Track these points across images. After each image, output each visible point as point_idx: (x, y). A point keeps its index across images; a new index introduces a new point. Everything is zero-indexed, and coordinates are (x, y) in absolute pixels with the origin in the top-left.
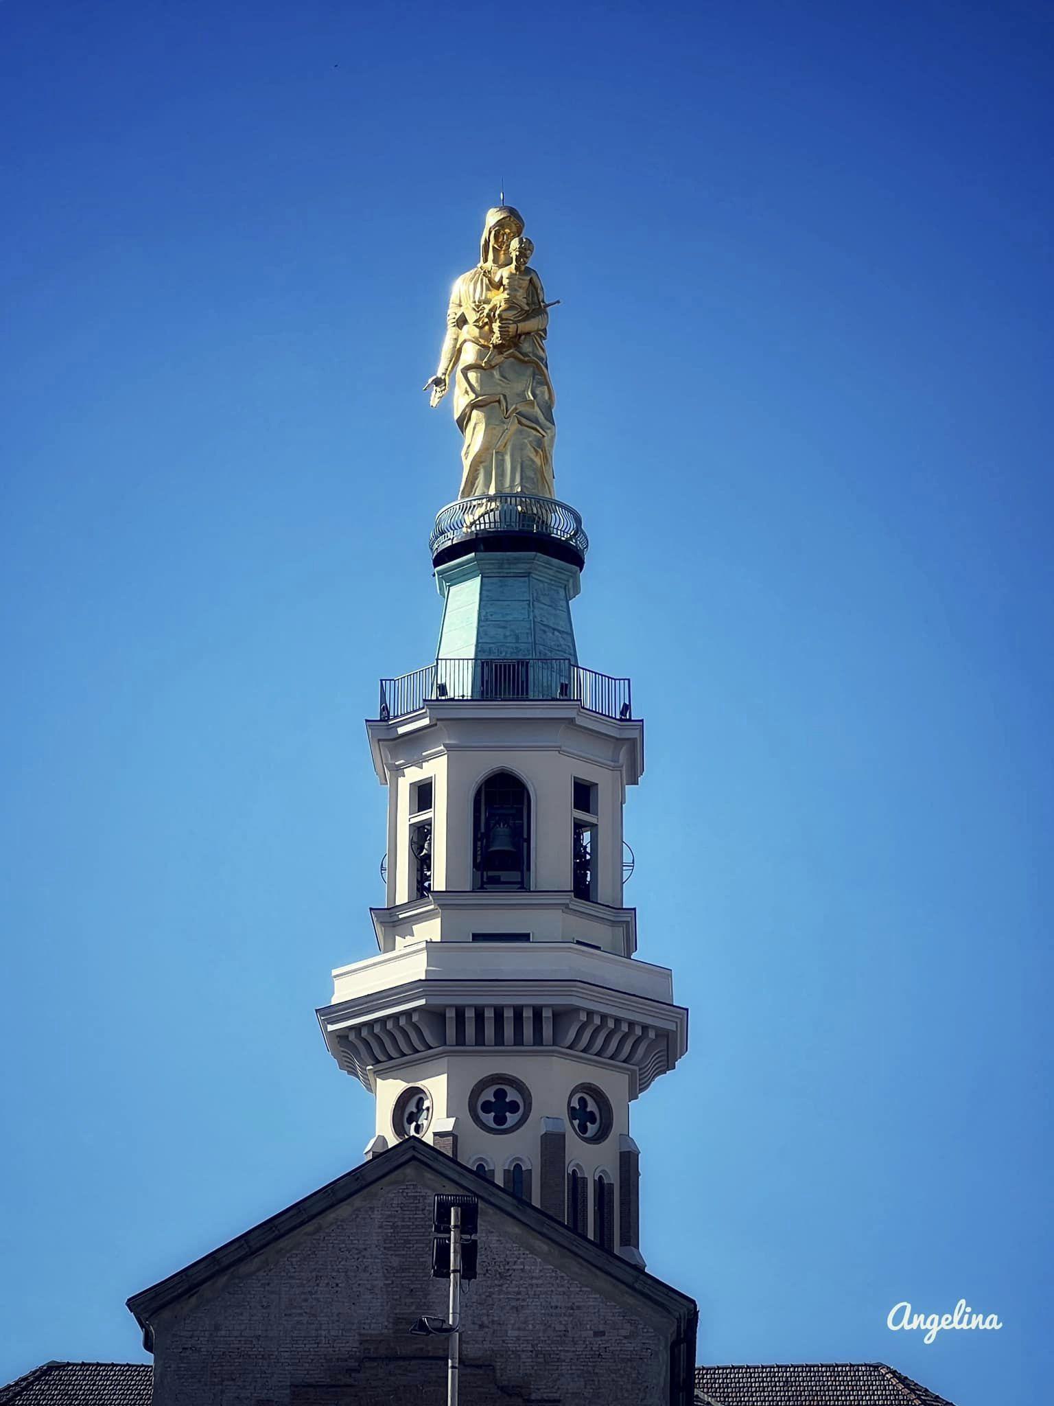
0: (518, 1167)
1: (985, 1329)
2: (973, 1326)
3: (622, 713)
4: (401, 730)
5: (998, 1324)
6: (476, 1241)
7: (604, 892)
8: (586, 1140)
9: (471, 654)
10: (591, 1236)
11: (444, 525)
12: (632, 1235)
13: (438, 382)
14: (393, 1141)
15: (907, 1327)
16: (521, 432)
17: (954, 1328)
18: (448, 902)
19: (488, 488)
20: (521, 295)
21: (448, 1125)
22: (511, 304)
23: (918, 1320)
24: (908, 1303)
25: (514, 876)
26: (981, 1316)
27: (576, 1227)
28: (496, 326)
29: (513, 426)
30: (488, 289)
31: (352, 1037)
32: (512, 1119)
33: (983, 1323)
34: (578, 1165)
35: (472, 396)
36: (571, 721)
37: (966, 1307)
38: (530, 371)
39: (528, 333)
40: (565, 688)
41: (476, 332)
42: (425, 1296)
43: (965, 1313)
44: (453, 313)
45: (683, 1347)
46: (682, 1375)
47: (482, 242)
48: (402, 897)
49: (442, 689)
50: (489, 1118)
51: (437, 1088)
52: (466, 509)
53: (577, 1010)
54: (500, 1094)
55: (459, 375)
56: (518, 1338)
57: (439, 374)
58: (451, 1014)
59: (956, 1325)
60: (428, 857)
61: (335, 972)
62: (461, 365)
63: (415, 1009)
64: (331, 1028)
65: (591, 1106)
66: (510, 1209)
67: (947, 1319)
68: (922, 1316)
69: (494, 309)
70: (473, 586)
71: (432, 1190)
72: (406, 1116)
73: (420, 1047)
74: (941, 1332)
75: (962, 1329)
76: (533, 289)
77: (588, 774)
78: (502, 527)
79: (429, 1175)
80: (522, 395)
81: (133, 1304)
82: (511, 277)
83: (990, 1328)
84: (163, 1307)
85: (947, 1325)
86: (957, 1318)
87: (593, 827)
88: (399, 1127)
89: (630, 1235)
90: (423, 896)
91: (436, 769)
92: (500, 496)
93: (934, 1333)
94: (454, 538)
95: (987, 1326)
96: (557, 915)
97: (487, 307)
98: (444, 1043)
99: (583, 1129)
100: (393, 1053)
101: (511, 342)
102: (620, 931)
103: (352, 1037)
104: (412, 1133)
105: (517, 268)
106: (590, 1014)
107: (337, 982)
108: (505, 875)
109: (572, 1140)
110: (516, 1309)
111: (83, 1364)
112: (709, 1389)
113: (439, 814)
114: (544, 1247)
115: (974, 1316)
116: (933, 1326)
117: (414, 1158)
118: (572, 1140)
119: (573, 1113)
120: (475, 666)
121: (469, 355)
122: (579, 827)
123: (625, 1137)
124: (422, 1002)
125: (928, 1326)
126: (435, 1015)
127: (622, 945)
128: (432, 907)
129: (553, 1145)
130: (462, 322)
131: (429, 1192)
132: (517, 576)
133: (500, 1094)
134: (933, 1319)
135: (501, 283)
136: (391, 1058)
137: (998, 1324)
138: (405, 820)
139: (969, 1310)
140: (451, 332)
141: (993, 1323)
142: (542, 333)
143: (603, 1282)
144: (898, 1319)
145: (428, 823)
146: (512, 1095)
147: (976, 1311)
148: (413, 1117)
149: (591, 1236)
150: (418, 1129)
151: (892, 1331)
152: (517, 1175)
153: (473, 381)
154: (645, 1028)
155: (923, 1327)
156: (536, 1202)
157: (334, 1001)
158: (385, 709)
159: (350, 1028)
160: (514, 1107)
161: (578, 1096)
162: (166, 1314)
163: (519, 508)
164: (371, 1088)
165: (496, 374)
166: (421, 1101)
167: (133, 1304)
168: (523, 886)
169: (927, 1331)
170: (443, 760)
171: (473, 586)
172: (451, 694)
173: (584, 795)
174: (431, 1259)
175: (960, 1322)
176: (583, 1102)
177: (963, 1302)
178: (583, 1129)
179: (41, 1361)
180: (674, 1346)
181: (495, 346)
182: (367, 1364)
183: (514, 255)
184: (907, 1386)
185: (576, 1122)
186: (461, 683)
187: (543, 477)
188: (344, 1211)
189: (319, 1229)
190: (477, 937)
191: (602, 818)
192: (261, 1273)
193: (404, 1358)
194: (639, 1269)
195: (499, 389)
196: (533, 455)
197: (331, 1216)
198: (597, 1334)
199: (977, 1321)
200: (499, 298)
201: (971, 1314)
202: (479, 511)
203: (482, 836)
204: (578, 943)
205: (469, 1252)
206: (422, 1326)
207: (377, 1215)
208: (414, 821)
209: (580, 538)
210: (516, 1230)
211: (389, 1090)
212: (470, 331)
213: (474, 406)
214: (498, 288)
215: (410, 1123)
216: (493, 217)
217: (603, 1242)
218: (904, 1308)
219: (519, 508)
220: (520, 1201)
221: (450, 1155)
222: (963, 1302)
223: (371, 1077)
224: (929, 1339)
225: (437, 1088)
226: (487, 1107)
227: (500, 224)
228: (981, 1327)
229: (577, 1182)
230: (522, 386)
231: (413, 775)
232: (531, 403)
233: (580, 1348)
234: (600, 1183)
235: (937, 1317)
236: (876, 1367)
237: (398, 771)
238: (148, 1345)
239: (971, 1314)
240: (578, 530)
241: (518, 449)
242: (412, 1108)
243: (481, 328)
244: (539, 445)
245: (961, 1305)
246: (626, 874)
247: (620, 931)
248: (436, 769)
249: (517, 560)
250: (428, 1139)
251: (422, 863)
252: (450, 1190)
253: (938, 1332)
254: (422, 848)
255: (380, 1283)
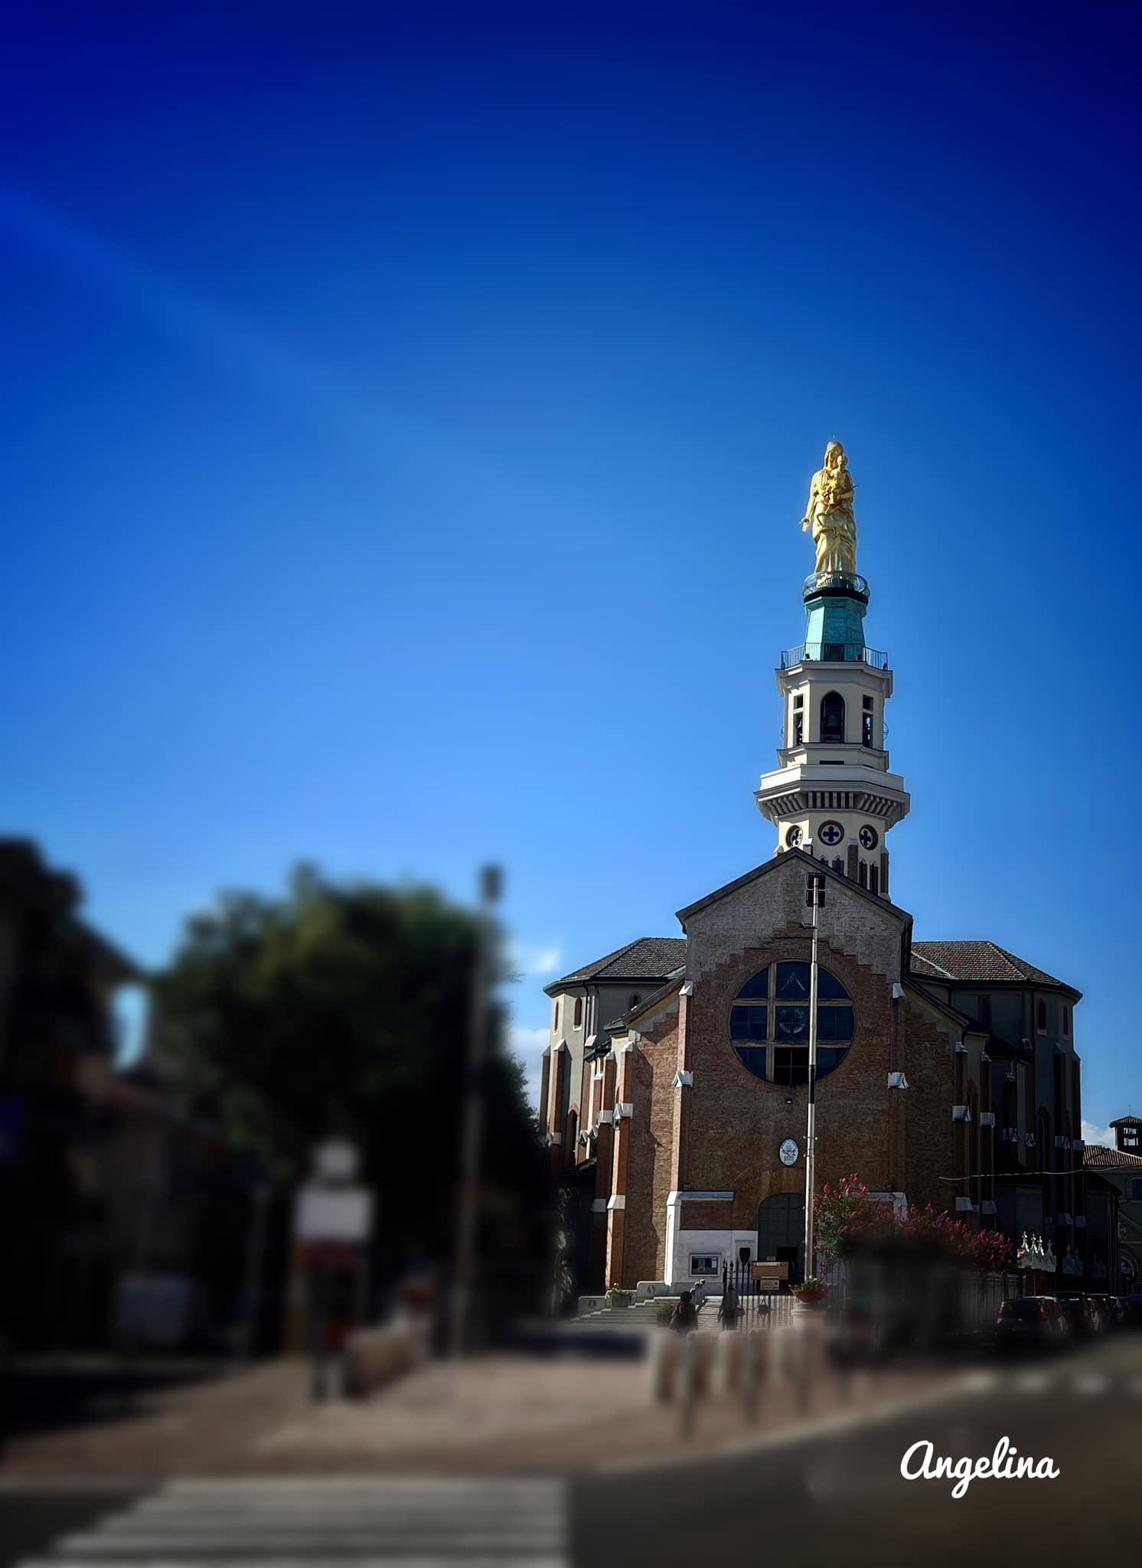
0: (838, 859)
1: (1036, 1477)
2: (1020, 1473)
3: (884, 667)
4: (790, 673)
5: (1054, 1470)
6: (573, 1111)
7: (875, 744)
8: (867, 848)
9: (820, 642)
10: (868, 888)
11: (808, 584)
12: (673, 1162)
13: (806, 521)
14: (786, 849)
15: (928, 1476)
16: (841, 543)
17: (993, 1476)
18: (810, 748)
19: (827, 568)
20: (842, 481)
21: (809, 841)
22: (838, 486)
23: (943, 1466)
24: (929, 1442)
25: (838, 737)
26: (1030, 1461)
27: (863, 884)
28: (831, 496)
29: (838, 541)
30: (828, 479)
31: (769, 804)
32: (836, 839)
33: (1034, 1470)
34: (863, 859)
35: (821, 527)
36: (862, 670)
37: (1009, 1448)
38: (846, 516)
39: (845, 500)
40: (860, 657)
41: (823, 498)
42: (800, 912)
43: (1008, 1455)
44: (813, 490)
45: (907, 934)
46: (906, 945)
47: (825, 458)
48: (790, 745)
49: (808, 656)
50: (826, 839)
51: (804, 826)
52: (819, 577)
53: (864, 794)
54: (831, 829)
55: (815, 518)
56: (838, 930)
57: (806, 517)
58: (811, 795)
59: (995, 1472)
60: (801, 728)
61: (762, 776)
62: (816, 514)
63: (795, 793)
64: (760, 800)
65: (869, 834)
66: (836, 877)
67: (983, 1464)
68: (949, 1461)
69: (831, 488)
70: (821, 611)
71: (805, 870)
72: (792, 837)
73: (792, 810)
74: (975, 1482)
75: (1004, 1477)
76: (847, 480)
77: (870, 693)
78: (833, 586)
79: (802, 863)
80: (843, 528)
81: (677, 914)
82: (838, 473)
83: (1041, 1476)
84: (689, 917)
85: (984, 1472)
86: (997, 1462)
87: (871, 716)
88: (789, 843)
89: (885, 889)
90: (799, 745)
91: (805, 690)
92: (833, 572)
93: (965, 1484)
94: (813, 590)
95: (1039, 1474)
96: (855, 754)
97: (828, 487)
98: (807, 807)
99: (866, 844)
100: (786, 811)
101: (838, 503)
102: (882, 760)
103: (769, 804)
104: (794, 845)
105: (841, 470)
106: (869, 795)
107: (763, 781)
108: (834, 736)
109: (861, 848)
110: (838, 918)
111: (657, 938)
112: (918, 951)
113: (806, 709)
114: (850, 893)
115: (1021, 1460)
116: (965, 1473)
117: (795, 856)
118: (861, 848)
119: (861, 837)
120: (821, 647)
121: (820, 509)
122: (865, 716)
123: (883, 847)
124: (799, 789)
125: (957, 1473)
126: (804, 795)
127: (882, 767)
128: (802, 749)
129: (853, 850)
130: (816, 494)
131: (802, 870)
132: (840, 607)
133: (831, 829)
134: (965, 1464)
135: (833, 476)
136: (785, 813)
137: (1054, 1470)
138: (792, 712)
139: (1013, 1451)
140: (812, 498)
141: (1046, 1469)
142: (851, 500)
143: (874, 908)
144: (915, 1464)
145: (802, 713)
146: (836, 829)
147: (1023, 1453)
148: (795, 838)
149: (868, 888)
150: (797, 843)
151: (904, 1478)
152: (838, 863)
153: (821, 521)
154: (892, 802)
155: (950, 1475)
156: (846, 874)
157: (762, 788)
158: (783, 664)
159: (768, 800)
160: (837, 834)
161: (863, 831)
162: (692, 919)
163: (841, 578)
164: (777, 826)
165: (831, 517)
166: (798, 832)
167: (677, 914)
168: (842, 741)
169: (956, 1480)
170: (808, 686)
171: (821, 611)
172: (811, 658)
173: (867, 702)
174: (805, 898)
175: (1002, 1468)
176: (865, 832)
177: (1005, 1440)
178: (866, 844)
179: (640, 937)
180: (903, 935)
181: (831, 505)
182: (776, 940)
183: (839, 463)
184: (998, 950)
185: (863, 841)
186: (815, 653)
187: (851, 564)
188: (766, 877)
189: (756, 884)
190: (822, 763)
191: (875, 713)
192: (732, 903)
193: (791, 938)
194: (889, 902)
195: (832, 525)
196: (846, 554)
197: (761, 879)
198: (871, 929)
199: (1025, 1466)
200: (833, 483)
201: (1016, 1458)
202: (824, 579)
203: (824, 720)
204: (864, 765)
205: (821, 896)
206: (802, 926)
207: (780, 879)
208: (795, 713)
209: (867, 590)
210: (838, 886)
211: (784, 827)
212: (820, 498)
213: (822, 532)
214: (832, 479)
215: (793, 840)
216: (830, 446)
217: (874, 891)
218: (924, 1448)
219: (841, 578)
220: (839, 873)
221: (810, 853)
222: (1005, 1440)
223: (777, 821)
224: (958, 1492)
225: (804, 826)
226: (825, 834)
227: (834, 449)
228: (1031, 1475)
229: (863, 866)
230: (842, 523)
231: (795, 693)
232: (846, 531)
233: (864, 934)
234: (872, 867)
235: (969, 1462)
236: (985, 942)
237: (789, 691)
238: (684, 931)
239: (1016, 1458)
240: (866, 587)
241: (840, 551)
242: (794, 834)
243: (825, 497)
244: (849, 550)
245: (1003, 1444)
246: (884, 737)
247: (882, 760)
248: (805, 690)
249: (840, 601)
250: (801, 847)
251: (799, 730)
252: (811, 870)
253: (971, 1482)
254: (799, 724)
255: (782, 907)
